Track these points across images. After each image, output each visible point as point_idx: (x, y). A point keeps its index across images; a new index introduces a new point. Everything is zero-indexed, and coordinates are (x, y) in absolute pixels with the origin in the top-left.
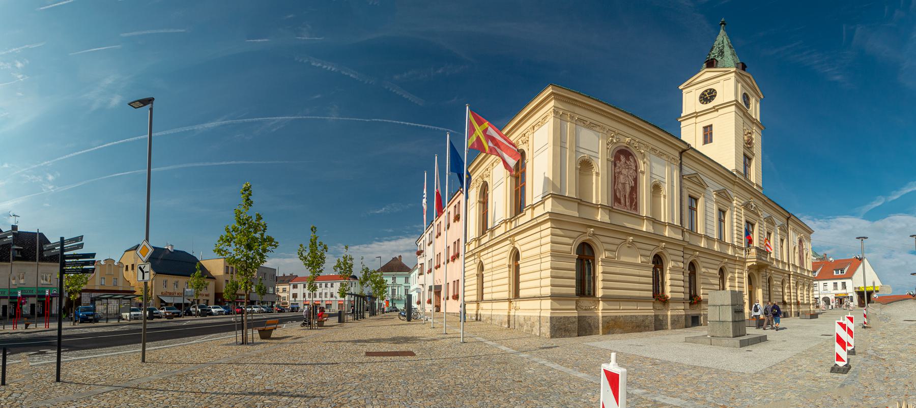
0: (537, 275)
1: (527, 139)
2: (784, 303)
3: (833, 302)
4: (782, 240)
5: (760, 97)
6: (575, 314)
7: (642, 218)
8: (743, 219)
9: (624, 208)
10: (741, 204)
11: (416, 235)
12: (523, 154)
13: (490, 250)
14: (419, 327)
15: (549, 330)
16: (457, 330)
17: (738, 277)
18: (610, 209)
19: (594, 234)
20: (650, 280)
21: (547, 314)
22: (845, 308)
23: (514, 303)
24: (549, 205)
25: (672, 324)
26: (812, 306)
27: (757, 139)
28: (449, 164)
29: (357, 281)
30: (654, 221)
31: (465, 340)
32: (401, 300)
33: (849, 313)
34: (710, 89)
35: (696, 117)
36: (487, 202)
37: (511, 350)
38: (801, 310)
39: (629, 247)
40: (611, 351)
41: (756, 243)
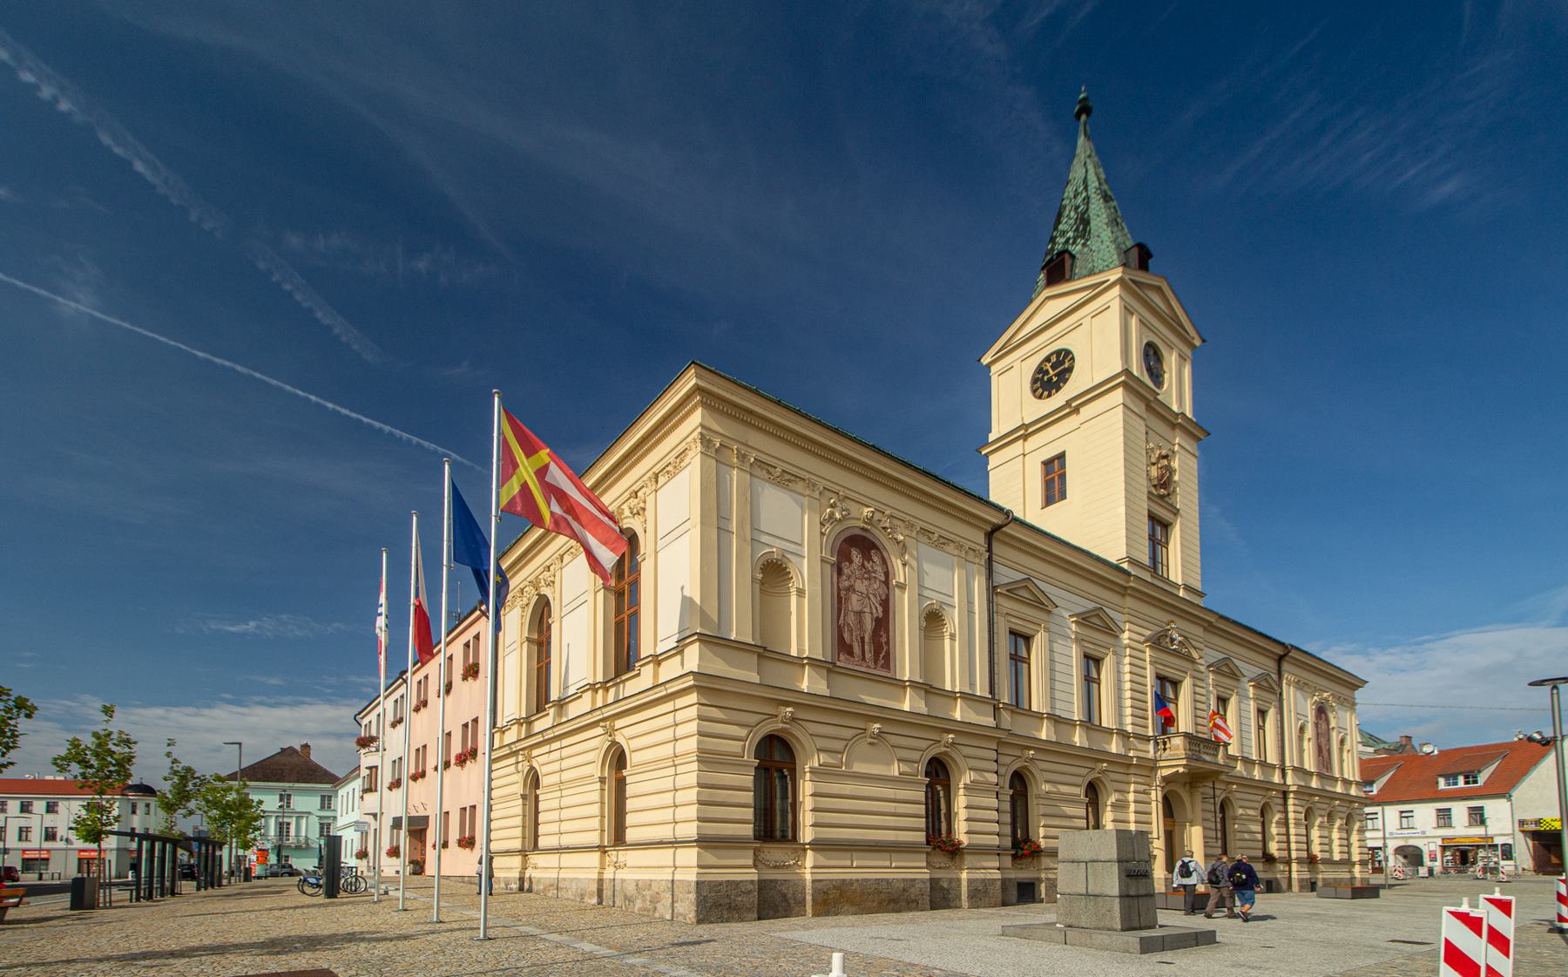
0: (667, 799)
1: (642, 505)
2: (1269, 859)
3: (1433, 859)
4: (1262, 713)
5: (1193, 347)
6: (752, 875)
7: (902, 684)
8: (1149, 672)
9: (860, 665)
10: (1142, 639)
11: (355, 700)
12: (632, 539)
13: (556, 745)
14: (361, 909)
16: (472, 913)
17: (1135, 802)
18: (829, 668)
19: (794, 719)
20: (921, 809)
21: (692, 876)
22: (1479, 874)
23: (613, 855)
24: (693, 657)
25: (971, 897)
26: (1357, 869)
27: (1185, 468)
28: (449, 541)
29: (153, 801)
30: (929, 689)
31: (491, 933)
32: (308, 847)
33: (1497, 889)
34: (1058, 353)
35: (1025, 437)
36: (549, 643)
37: (604, 951)
38: (1320, 876)
39: (871, 744)
40: (833, 950)
41: (1184, 722)
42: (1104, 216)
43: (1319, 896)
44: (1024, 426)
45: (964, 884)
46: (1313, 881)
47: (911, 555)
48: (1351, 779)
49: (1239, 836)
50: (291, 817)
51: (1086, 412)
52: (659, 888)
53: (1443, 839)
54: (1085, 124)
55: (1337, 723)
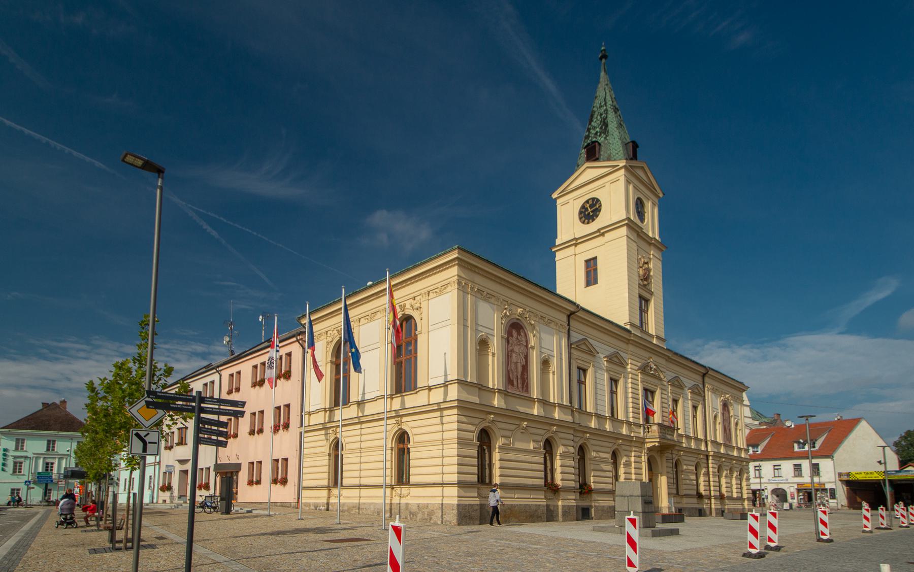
3: (793, 498)
4: (695, 408)
5: (658, 197)
7: (533, 400)
8: (640, 387)
10: (636, 368)
15: (456, 518)
17: (634, 462)
18: (504, 393)
21: (455, 501)
26: (746, 503)
27: (655, 267)
30: (544, 402)
34: (593, 199)
35: (576, 245)
42: (615, 123)
43: (724, 518)
44: (575, 239)
45: (560, 508)
46: (723, 510)
47: (537, 330)
48: (742, 447)
49: (684, 482)
50: (55, 458)
51: (608, 236)
52: (433, 507)
53: (798, 484)
54: (604, 64)
55: (734, 413)
